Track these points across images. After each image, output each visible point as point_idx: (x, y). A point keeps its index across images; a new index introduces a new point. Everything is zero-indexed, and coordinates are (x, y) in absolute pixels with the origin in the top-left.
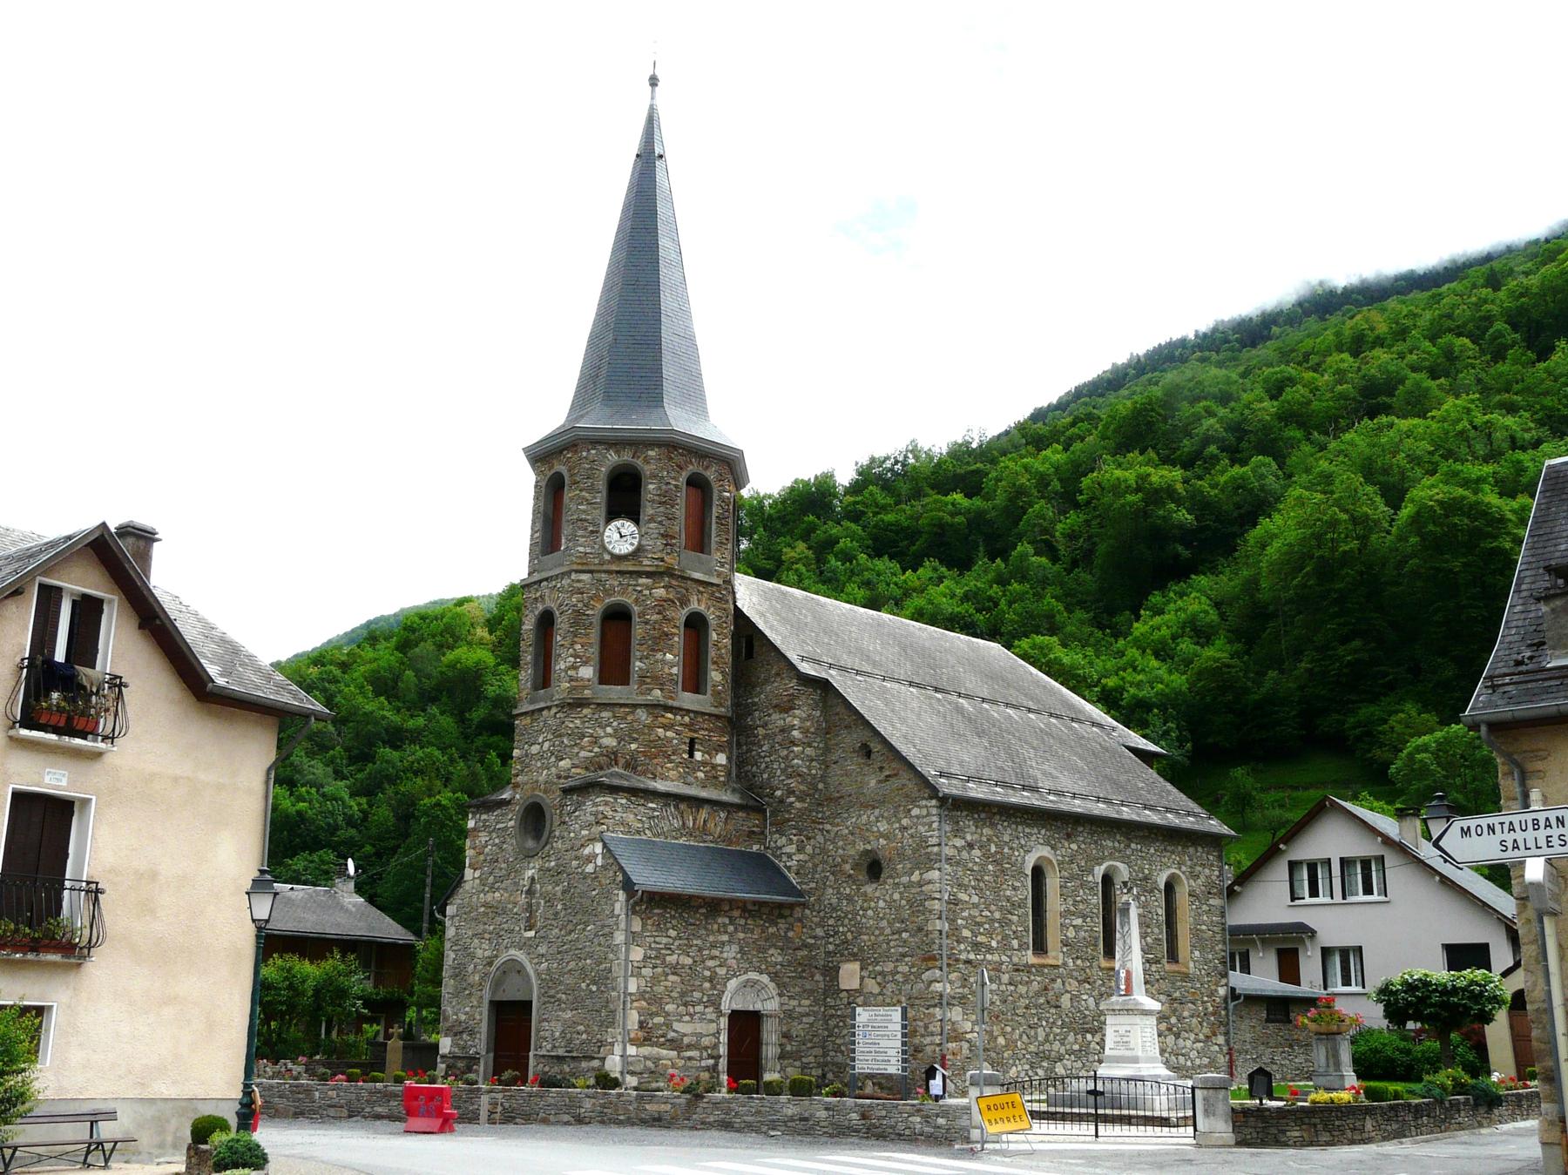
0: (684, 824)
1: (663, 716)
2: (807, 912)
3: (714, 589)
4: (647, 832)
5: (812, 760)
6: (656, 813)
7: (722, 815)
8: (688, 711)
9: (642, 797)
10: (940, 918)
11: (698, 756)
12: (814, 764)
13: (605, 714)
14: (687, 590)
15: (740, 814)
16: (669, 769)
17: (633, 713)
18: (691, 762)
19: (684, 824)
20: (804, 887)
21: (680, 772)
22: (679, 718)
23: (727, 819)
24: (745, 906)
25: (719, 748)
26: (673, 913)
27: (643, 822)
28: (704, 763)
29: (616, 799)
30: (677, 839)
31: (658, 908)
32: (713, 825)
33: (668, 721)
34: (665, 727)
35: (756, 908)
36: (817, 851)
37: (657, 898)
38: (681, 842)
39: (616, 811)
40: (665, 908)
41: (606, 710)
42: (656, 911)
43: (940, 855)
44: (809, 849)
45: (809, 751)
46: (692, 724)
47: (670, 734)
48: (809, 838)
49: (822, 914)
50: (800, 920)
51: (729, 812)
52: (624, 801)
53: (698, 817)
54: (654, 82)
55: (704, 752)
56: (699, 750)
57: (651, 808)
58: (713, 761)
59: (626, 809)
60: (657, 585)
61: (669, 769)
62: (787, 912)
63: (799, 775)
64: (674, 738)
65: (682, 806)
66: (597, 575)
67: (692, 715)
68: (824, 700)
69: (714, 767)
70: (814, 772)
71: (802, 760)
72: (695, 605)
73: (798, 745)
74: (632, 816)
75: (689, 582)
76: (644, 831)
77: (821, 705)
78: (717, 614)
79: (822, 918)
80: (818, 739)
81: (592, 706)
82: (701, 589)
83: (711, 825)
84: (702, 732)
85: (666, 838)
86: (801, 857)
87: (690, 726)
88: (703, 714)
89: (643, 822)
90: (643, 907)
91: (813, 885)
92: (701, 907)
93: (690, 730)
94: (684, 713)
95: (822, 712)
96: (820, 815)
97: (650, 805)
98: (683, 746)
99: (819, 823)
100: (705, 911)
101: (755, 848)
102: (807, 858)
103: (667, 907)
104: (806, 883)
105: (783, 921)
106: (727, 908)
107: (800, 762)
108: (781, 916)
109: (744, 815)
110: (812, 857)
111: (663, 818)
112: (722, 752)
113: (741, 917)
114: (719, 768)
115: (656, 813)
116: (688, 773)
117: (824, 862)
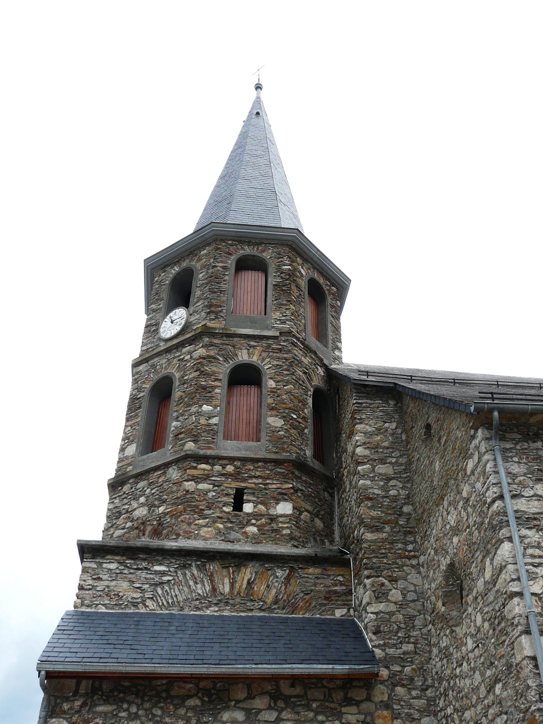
0: (214, 589)
1: (195, 468)
2: (400, 690)
3: (270, 342)
4: (149, 603)
5: (389, 479)
6: (166, 578)
7: (279, 573)
8: (231, 460)
9: (144, 560)
10: (528, 632)
11: (248, 508)
12: (392, 483)
13: (141, 484)
14: (234, 346)
15: (311, 570)
16: (200, 527)
17: (164, 473)
18: (236, 515)
19: (214, 589)
20: (391, 651)
21: (218, 529)
22: (218, 468)
23: (288, 579)
24: (278, 689)
25: (282, 496)
26: (134, 709)
27: (143, 591)
28: (257, 516)
29: (100, 564)
30: (198, 609)
31: (107, 702)
32: (263, 587)
33: (202, 472)
34: (196, 479)
35: (298, 690)
36: (411, 596)
37: (84, 685)
38: (208, 612)
39: (100, 579)
40: (118, 702)
41: (142, 480)
42: (100, 709)
43: (505, 514)
44: (395, 595)
45: (381, 469)
46: (239, 473)
47: (203, 486)
48: (393, 580)
49: (429, 693)
50: (387, 706)
51: (292, 569)
52: (113, 566)
53: (239, 579)
54: (258, 87)
55: (256, 504)
56: (249, 501)
57: (157, 573)
58: (272, 512)
59: (115, 575)
60: (198, 347)
61: (200, 527)
62: (359, 694)
63: (371, 499)
64: (210, 491)
65: (212, 567)
66: (150, 362)
67: (238, 463)
68: (401, 411)
69: (273, 519)
70: (393, 492)
71: (372, 479)
72: (243, 356)
73: (363, 463)
74: (125, 585)
75: (236, 339)
76: (143, 602)
77: (396, 416)
78: (275, 363)
79: (431, 701)
80: (396, 454)
81: (131, 481)
82: (252, 343)
83: (260, 588)
84: (254, 480)
85: (182, 609)
86: (381, 607)
87: (236, 476)
88: (257, 460)
89: (143, 591)
90: (78, 703)
91: (410, 647)
92: (190, 697)
93: (236, 479)
94: (224, 462)
95: (399, 423)
96: (410, 547)
97: (157, 568)
98: (225, 499)
99: (409, 558)
100: (198, 702)
101: (339, 613)
102: (392, 608)
103: (123, 701)
104: (394, 646)
105: (353, 709)
106: (242, 695)
107: (368, 482)
108: (349, 701)
109: (318, 571)
110: (401, 605)
111: (179, 584)
112: (285, 500)
113: (270, 708)
114: (281, 519)
115: (166, 578)
116: (231, 528)
117: (422, 611)
